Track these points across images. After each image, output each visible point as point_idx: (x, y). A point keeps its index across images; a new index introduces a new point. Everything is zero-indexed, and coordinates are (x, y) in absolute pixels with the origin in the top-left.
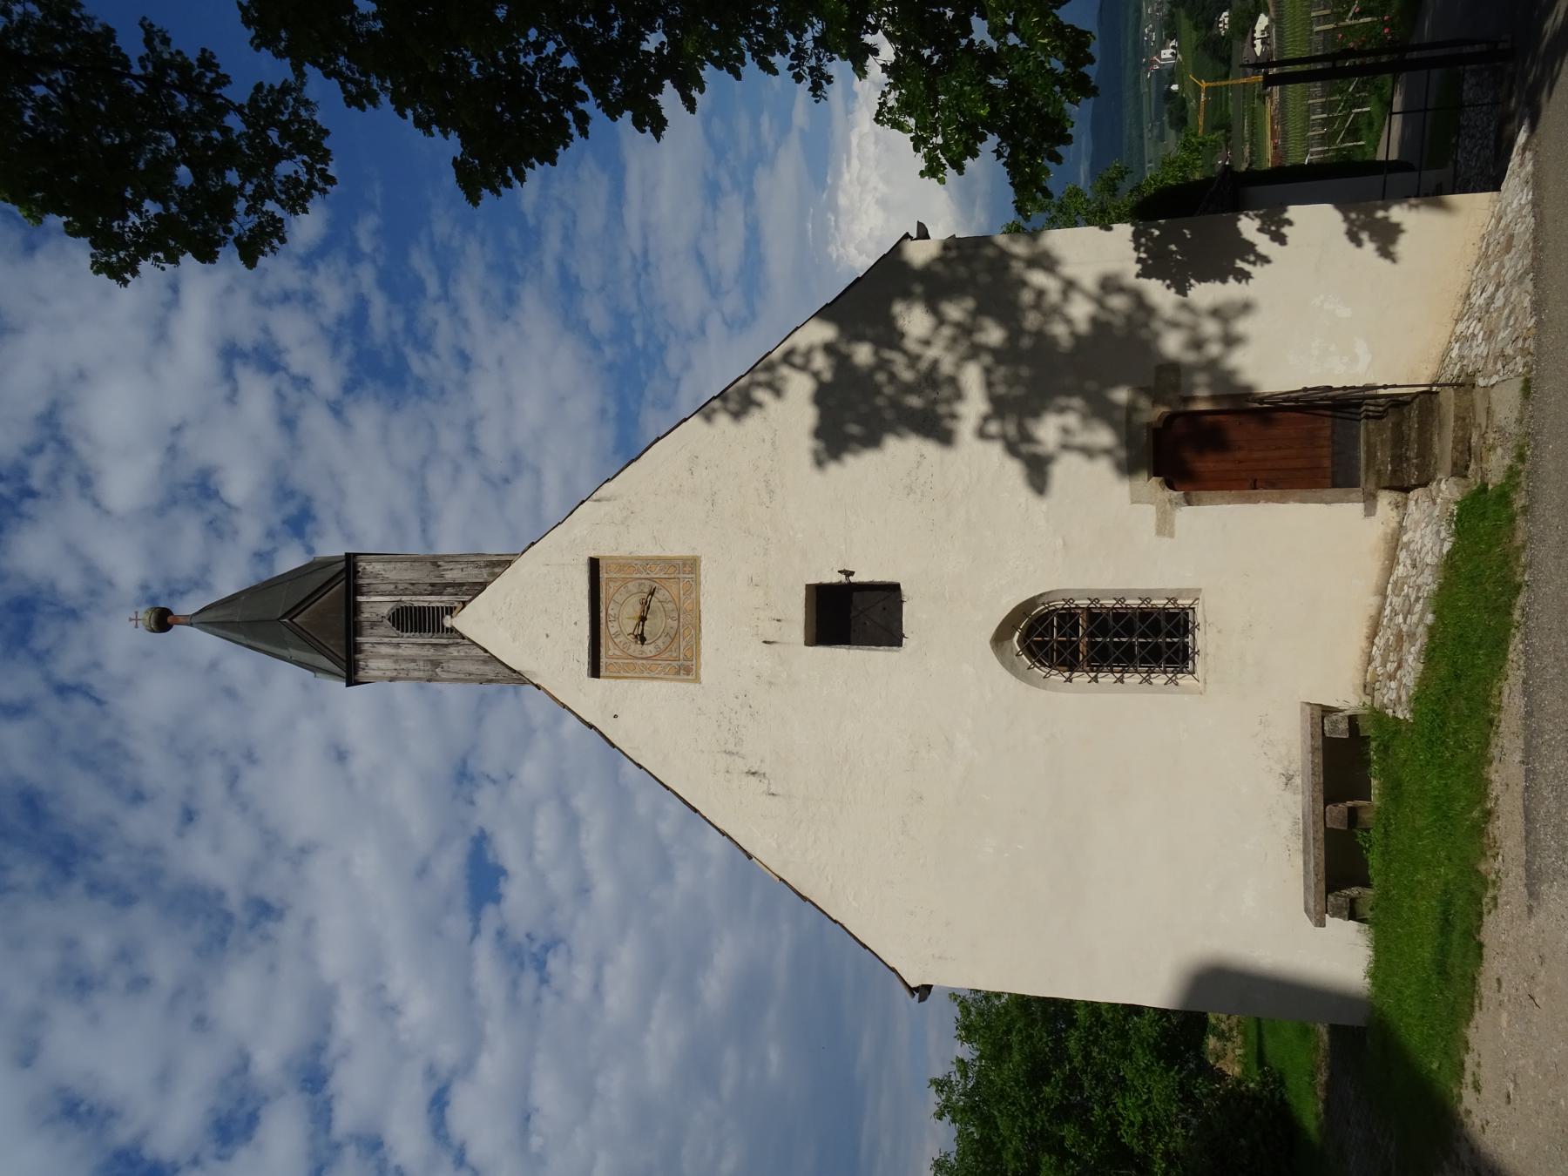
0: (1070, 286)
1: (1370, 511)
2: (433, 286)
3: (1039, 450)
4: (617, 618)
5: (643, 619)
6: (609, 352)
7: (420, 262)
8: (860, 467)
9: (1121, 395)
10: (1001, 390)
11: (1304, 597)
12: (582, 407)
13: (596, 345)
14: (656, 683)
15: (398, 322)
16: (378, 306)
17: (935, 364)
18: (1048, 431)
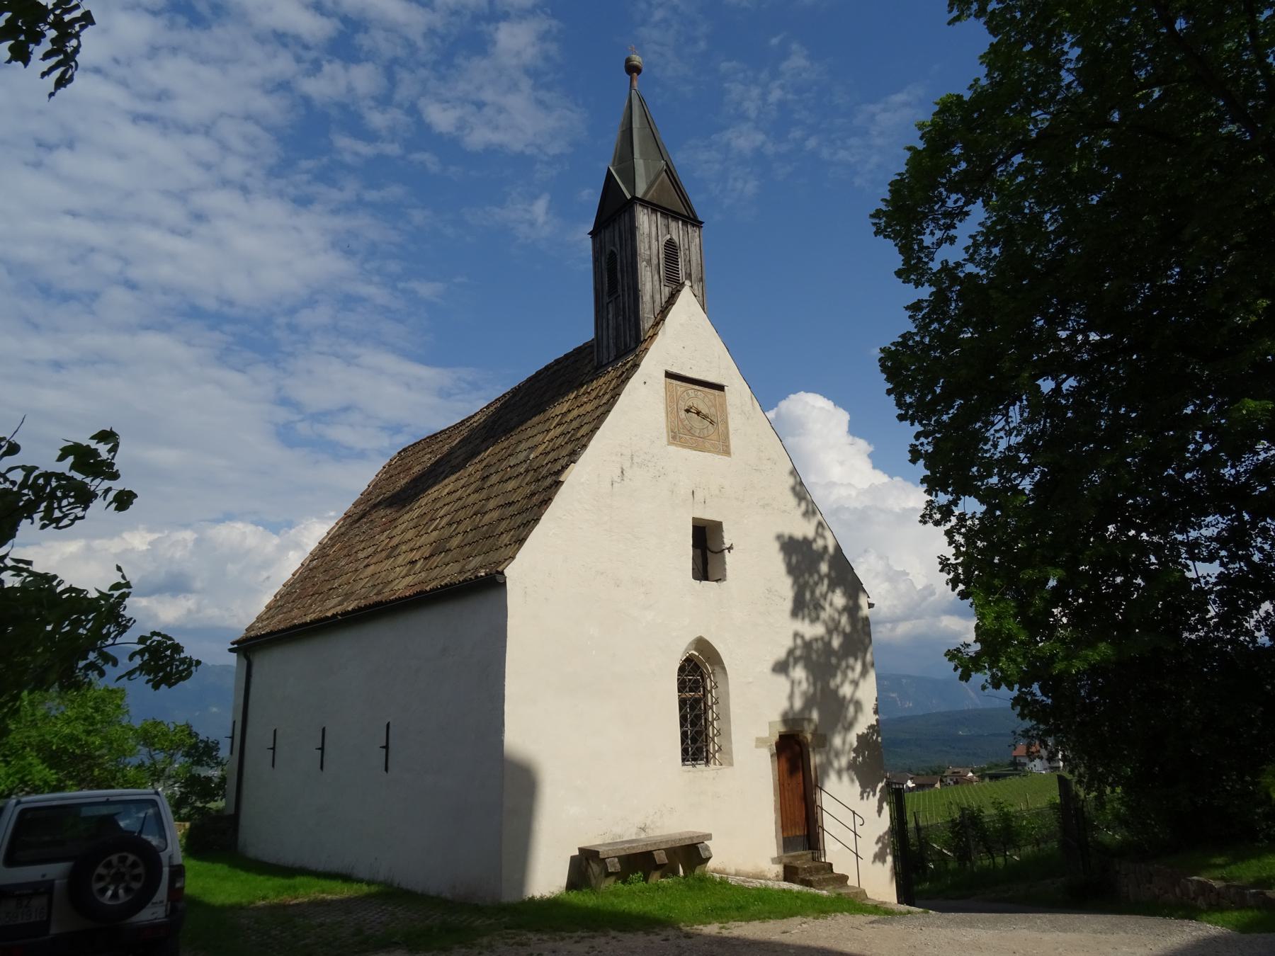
0: (855, 684)
1: (774, 861)
2: (372, 195)
3: (791, 669)
4: (696, 396)
5: (698, 413)
6: (282, 320)
7: (395, 191)
8: (777, 562)
9: (815, 715)
10: (815, 646)
11: (737, 825)
12: (239, 287)
13: (293, 311)
14: (664, 415)
15: (348, 158)
16: (365, 149)
17: (823, 609)
18: (799, 673)
